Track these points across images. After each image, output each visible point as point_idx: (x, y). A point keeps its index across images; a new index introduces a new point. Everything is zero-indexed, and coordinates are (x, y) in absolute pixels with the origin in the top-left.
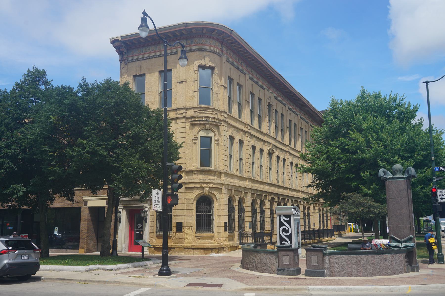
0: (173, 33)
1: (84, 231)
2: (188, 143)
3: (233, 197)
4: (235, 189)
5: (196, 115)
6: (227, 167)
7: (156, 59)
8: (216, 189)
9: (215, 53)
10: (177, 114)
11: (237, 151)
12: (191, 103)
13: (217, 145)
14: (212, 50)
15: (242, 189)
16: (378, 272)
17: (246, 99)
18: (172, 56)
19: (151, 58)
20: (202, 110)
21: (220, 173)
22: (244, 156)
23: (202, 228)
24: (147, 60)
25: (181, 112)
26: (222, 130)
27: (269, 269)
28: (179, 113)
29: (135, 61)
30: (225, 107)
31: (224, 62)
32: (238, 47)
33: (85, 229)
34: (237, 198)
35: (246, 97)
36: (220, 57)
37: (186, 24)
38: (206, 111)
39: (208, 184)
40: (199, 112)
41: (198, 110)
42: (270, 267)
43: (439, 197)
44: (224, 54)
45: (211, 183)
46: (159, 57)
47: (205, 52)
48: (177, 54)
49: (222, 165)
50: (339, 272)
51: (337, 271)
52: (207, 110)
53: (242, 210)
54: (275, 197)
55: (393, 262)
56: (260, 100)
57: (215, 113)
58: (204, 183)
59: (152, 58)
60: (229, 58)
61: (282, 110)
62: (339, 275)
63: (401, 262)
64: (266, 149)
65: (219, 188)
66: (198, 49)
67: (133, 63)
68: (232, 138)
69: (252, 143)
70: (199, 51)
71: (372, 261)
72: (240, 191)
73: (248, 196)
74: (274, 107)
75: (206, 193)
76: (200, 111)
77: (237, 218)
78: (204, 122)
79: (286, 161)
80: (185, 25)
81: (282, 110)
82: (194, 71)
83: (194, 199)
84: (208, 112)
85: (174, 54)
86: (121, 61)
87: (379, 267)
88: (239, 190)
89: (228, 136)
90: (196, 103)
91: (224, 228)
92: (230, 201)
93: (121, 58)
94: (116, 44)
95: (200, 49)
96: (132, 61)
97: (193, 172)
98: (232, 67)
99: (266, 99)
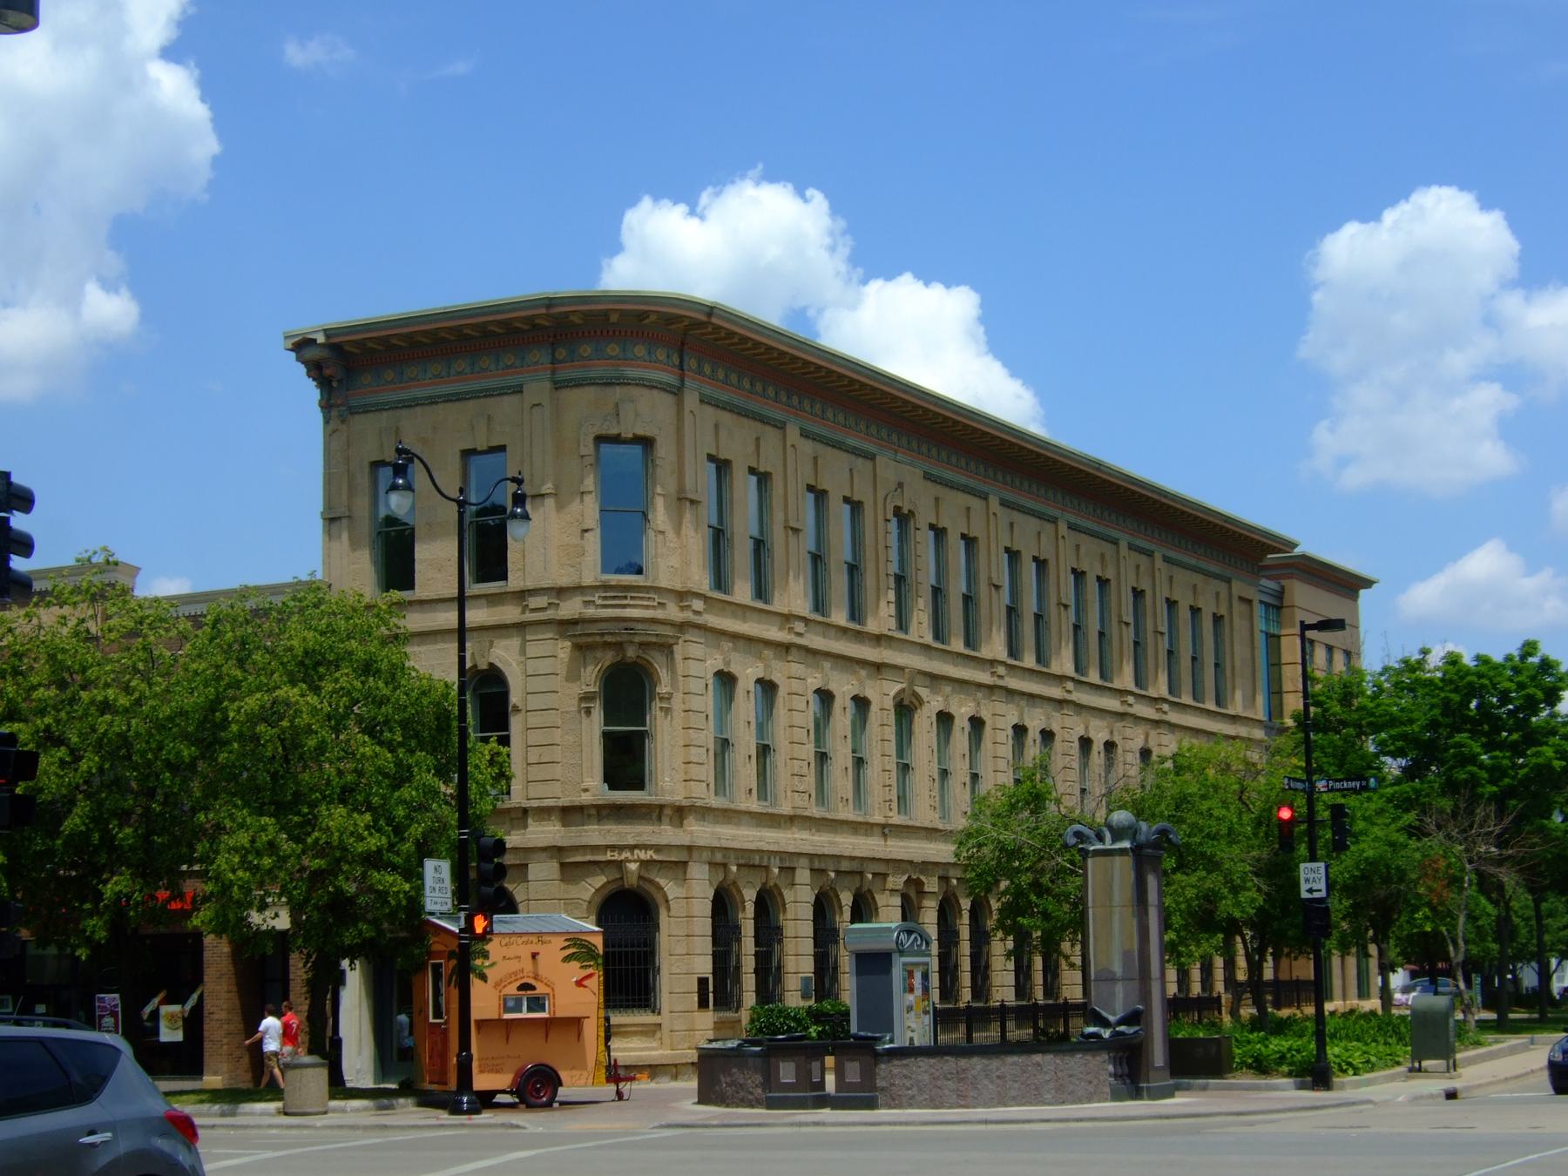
0: (507, 325)
1: (216, 1017)
2: (567, 709)
3: (732, 887)
4: (742, 861)
5: (591, 612)
6: (705, 784)
7: (450, 405)
8: (664, 864)
9: (656, 387)
10: (527, 612)
11: (749, 723)
12: (572, 570)
13: (666, 714)
14: (643, 379)
15: (769, 859)
16: (1014, 1098)
17: (786, 521)
18: (506, 398)
19: (432, 401)
20: (612, 594)
21: (680, 813)
22: (780, 738)
23: (624, 997)
24: (419, 409)
25: (540, 602)
26: (685, 659)
27: (750, 1097)
28: (532, 606)
29: (377, 410)
30: (700, 579)
31: (691, 412)
32: (321, 1148)
33: (222, 1010)
34: (750, 895)
35: (786, 514)
36: (675, 394)
37: (550, 302)
38: (626, 598)
39: (636, 851)
40: (600, 602)
41: (597, 595)
42: (751, 1093)
43: (1304, 887)
44: (688, 382)
45: (645, 847)
46: (458, 400)
47: (618, 387)
48: (521, 392)
49: (686, 781)
50: (913, 1097)
51: (906, 1095)
52: (629, 595)
53: (769, 932)
54: (923, 878)
55: (1059, 1074)
56: (856, 506)
57: (655, 604)
58: (621, 848)
59: (437, 403)
60: (708, 390)
61: (968, 518)
62: (911, 1106)
63: (1088, 1074)
64: (883, 694)
65: (676, 863)
66: (595, 378)
67: (370, 415)
68: (726, 680)
69: (815, 681)
70: (597, 384)
71: (998, 1069)
72: (760, 866)
73: (798, 880)
74: (925, 516)
75: (632, 881)
76: (605, 598)
77: (749, 963)
78: (619, 639)
79: (988, 729)
80: (547, 302)
81: (968, 518)
82: (582, 456)
83: (590, 902)
84: (632, 602)
85: (513, 393)
86: (326, 406)
87: (1016, 1085)
88: (757, 863)
89: (710, 675)
90: (591, 572)
91: (696, 999)
92: (723, 905)
93: (326, 396)
94: (311, 353)
95: (602, 378)
96: (366, 410)
97: (586, 812)
98: (726, 417)
99: (881, 494)
